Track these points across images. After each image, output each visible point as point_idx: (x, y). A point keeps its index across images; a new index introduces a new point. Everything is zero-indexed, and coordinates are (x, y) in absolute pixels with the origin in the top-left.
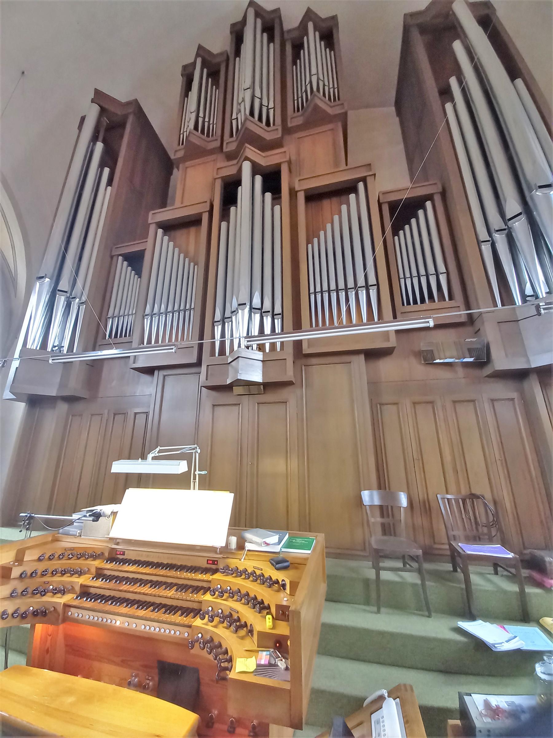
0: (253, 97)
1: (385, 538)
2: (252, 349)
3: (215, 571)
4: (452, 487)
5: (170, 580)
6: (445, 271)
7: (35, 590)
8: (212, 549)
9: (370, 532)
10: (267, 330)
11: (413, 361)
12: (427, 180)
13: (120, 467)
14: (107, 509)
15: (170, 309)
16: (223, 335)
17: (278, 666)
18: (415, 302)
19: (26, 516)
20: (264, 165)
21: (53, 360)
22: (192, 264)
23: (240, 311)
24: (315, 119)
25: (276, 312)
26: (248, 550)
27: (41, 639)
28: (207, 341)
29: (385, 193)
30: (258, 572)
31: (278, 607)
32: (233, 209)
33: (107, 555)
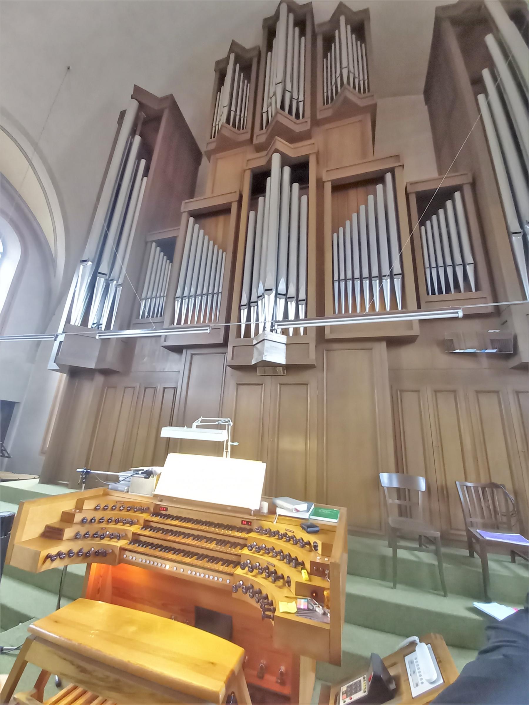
0: (284, 90)
1: (402, 519)
2: (276, 333)
3: (250, 531)
4: (472, 474)
5: (209, 535)
6: (472, 261)
7: (95, 534)
8: (247, 511)
9: (387, 512)
10: (292, 315)
11: (437, 351)
12: (456, 171)
13: (167, 432)
14: (156, 469)
15: (199, 292)
16: (249, 319)
17: (315, 611)
18: (440, 292)
19: (83, 472)
20: (293, 156)
21: (99, 336)
22: (221, 251)
23: (266, 296)
24: (345, 111)
25: (300, 298)
26: (279, 515)
27: (95, 579)
28: (233, 324)
29: (412, 184)
30: (290, 534)
31: (313, 563)
32: (261, 199)
33: (152, 509)
